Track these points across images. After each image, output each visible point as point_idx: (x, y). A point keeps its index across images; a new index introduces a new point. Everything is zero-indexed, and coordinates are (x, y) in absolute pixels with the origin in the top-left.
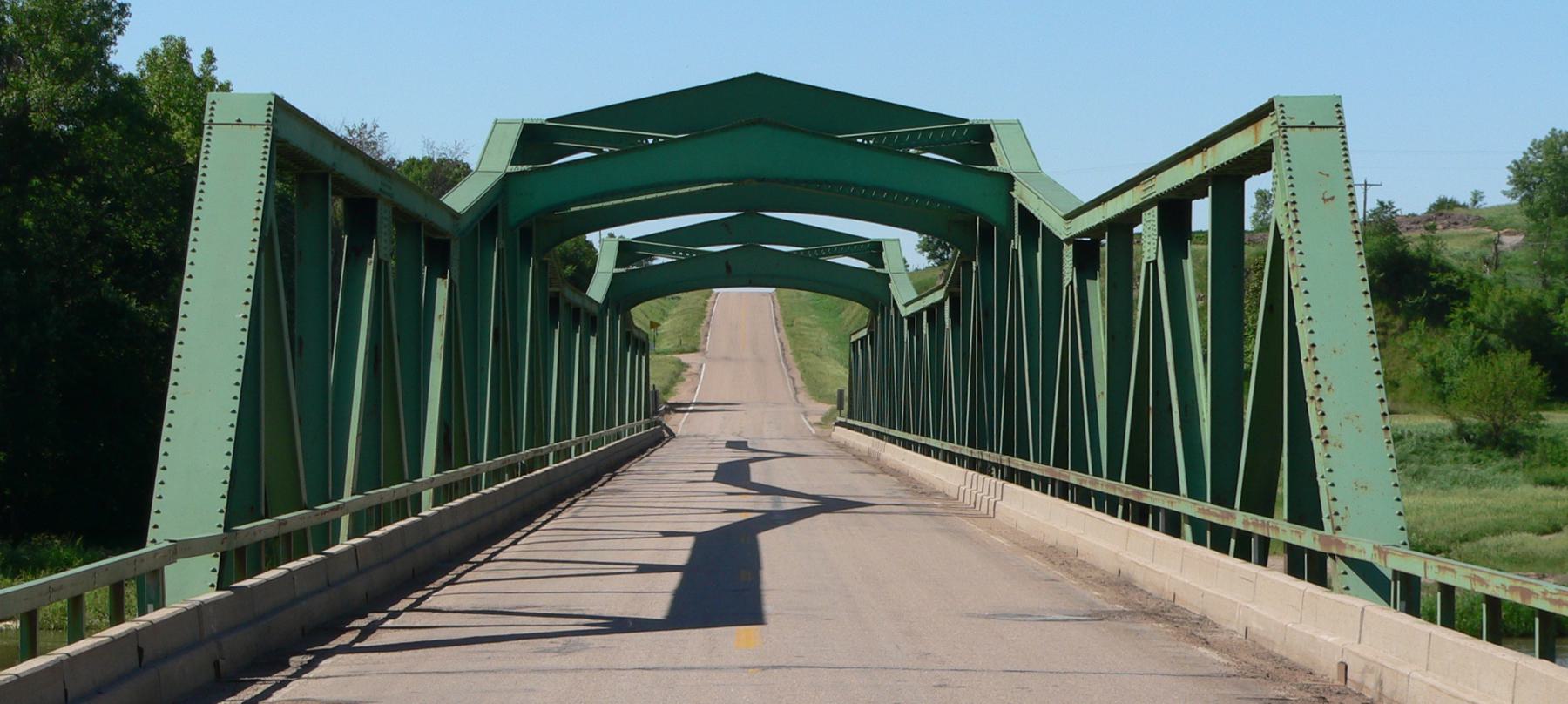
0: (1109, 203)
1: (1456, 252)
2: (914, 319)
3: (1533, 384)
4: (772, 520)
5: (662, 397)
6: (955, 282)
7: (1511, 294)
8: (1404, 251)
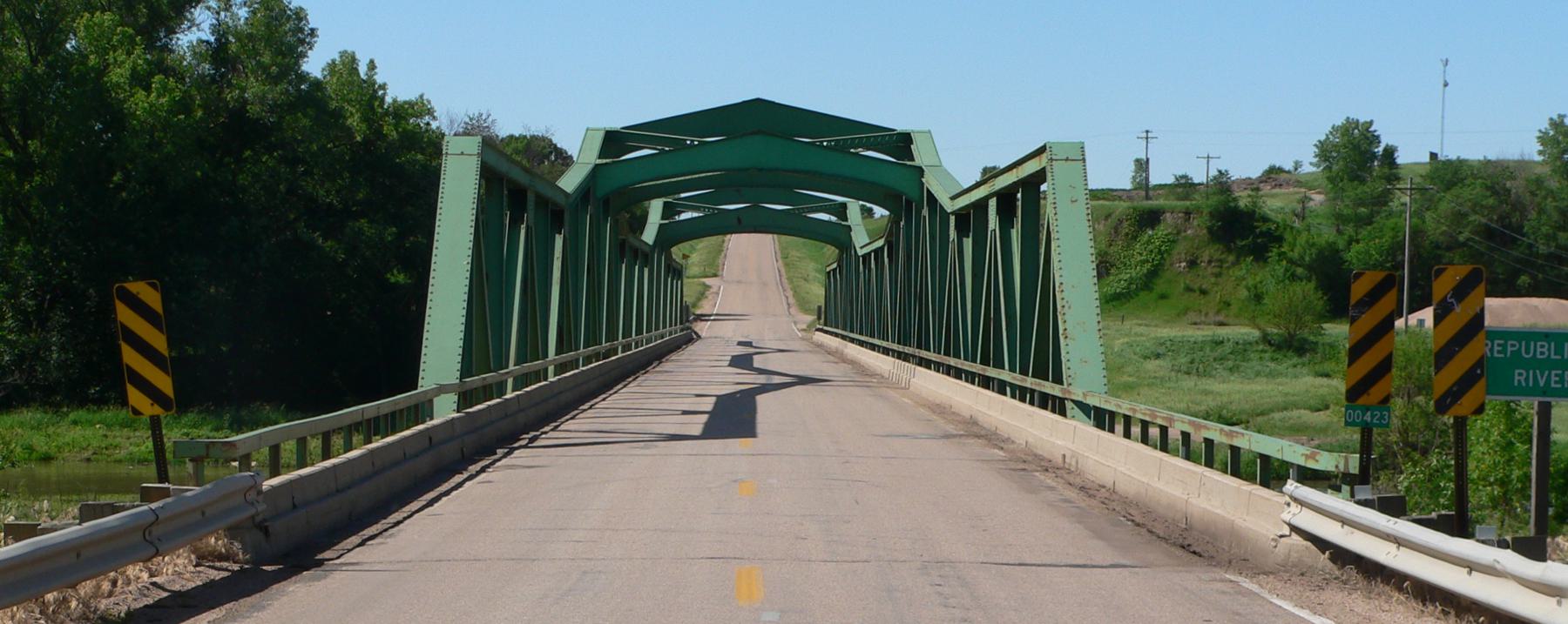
0: (1024, 165)
1: (1274, 207)
2: (866, 257)
4: (765, 389)
5: (692, 310)
6: (890, 234)
7: (1313, 238)
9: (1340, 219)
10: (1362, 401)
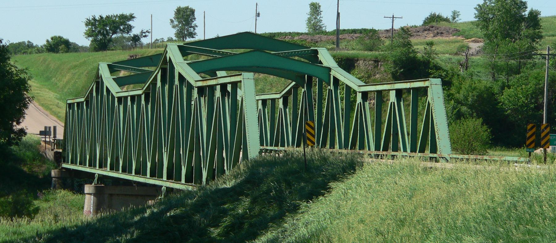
3: (483, 135)
7: (475, 83)
8: (414, 57)
9: (495, 69)
10: (529, 147)
